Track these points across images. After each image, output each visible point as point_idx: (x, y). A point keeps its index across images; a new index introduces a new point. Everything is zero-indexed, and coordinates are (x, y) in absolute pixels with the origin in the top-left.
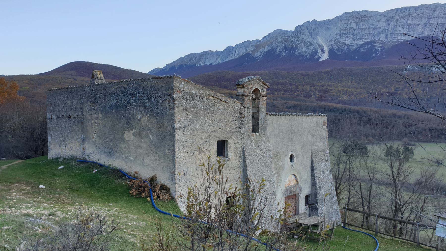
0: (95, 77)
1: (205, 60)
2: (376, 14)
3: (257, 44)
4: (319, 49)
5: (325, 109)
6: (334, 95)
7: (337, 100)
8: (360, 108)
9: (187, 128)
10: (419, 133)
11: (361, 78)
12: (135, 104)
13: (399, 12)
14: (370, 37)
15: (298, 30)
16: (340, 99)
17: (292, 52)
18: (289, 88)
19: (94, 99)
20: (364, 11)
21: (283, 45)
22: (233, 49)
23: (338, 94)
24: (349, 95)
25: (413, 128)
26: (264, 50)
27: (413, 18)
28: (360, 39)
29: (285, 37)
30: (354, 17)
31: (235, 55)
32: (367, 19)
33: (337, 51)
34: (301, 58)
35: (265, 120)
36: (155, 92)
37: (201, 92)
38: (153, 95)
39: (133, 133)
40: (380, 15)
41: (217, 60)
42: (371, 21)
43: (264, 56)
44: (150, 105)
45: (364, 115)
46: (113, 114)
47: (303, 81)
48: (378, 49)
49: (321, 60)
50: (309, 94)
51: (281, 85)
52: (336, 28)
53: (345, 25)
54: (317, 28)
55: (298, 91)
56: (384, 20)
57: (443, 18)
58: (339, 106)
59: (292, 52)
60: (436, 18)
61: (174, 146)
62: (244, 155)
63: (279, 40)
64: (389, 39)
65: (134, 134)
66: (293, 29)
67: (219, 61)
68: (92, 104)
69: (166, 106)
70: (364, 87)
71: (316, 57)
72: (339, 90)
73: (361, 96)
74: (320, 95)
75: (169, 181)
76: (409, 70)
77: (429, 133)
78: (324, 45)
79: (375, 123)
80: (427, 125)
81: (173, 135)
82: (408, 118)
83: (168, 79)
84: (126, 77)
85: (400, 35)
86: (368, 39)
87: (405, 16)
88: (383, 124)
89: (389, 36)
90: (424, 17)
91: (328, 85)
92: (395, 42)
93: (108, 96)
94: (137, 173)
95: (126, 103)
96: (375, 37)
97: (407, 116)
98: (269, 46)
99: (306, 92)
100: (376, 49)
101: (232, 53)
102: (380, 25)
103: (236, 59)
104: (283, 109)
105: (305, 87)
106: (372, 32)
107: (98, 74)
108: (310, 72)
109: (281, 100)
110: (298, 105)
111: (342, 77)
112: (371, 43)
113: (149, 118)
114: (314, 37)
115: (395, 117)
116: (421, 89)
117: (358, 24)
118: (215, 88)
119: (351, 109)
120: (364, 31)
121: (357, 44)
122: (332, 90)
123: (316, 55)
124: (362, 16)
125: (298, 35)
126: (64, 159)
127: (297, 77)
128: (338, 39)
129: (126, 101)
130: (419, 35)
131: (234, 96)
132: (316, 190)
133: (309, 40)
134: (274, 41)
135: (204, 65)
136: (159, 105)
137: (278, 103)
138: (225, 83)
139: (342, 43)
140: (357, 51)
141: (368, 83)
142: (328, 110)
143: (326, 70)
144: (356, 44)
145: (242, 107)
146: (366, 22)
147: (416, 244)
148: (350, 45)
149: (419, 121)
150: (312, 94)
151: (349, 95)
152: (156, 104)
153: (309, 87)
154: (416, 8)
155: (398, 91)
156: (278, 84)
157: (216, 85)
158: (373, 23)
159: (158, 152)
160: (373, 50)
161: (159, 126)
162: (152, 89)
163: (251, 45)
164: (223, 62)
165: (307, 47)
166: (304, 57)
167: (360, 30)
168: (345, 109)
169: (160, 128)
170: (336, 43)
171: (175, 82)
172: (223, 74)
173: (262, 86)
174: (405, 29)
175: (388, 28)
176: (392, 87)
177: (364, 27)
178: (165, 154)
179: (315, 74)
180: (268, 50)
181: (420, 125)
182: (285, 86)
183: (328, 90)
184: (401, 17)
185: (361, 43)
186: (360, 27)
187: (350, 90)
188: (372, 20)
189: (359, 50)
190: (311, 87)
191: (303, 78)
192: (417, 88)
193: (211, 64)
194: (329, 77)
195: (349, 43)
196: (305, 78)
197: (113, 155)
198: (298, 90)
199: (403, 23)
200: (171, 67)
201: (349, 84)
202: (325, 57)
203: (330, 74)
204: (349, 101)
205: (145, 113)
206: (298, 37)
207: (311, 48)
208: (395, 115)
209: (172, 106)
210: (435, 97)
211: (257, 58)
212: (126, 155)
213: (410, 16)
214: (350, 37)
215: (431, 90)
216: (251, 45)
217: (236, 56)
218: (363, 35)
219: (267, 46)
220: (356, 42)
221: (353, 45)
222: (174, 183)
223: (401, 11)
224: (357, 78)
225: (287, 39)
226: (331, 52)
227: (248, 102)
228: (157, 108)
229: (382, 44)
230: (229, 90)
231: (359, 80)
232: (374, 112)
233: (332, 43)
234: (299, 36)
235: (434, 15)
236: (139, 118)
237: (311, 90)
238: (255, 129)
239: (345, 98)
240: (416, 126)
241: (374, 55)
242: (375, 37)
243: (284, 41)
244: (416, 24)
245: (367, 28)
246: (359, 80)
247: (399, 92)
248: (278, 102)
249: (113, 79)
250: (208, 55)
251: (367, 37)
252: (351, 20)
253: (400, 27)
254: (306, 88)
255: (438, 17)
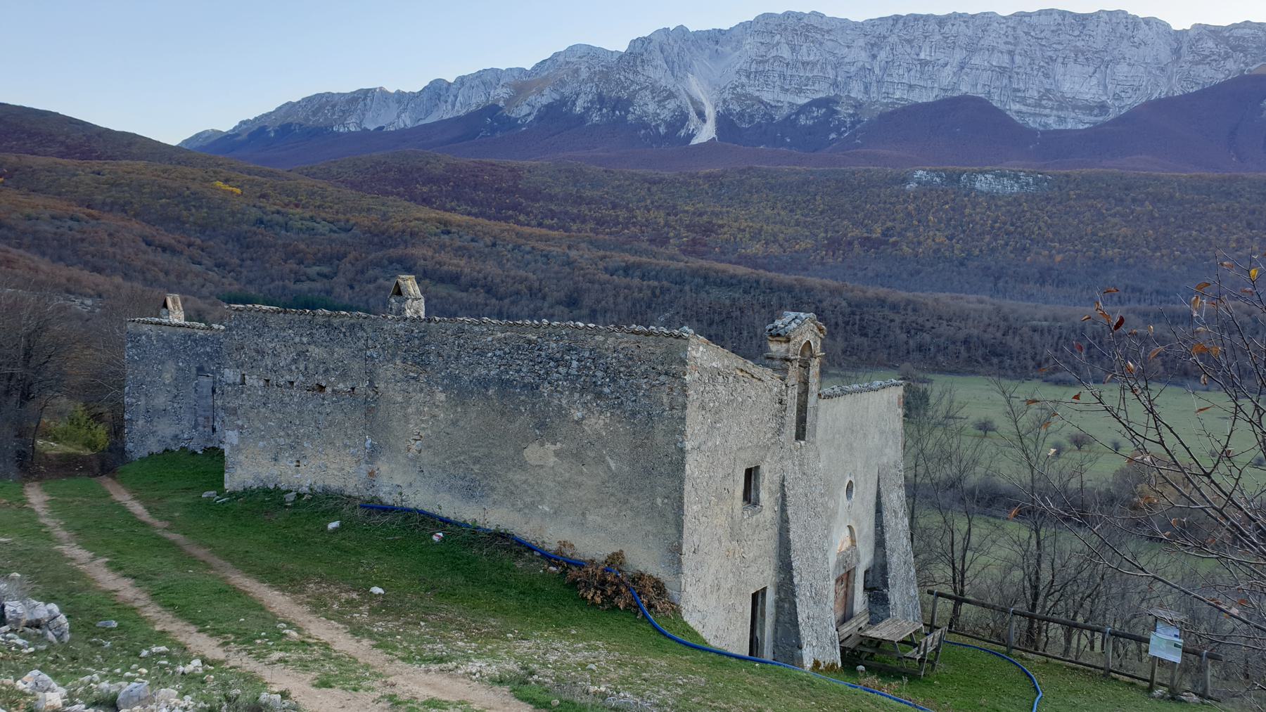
0: (405, 294)
1: (363, 114)
2: (845, 25)
3: (522, 82)
4: (691, 109)
5: (705, 278)
6: (727, 241)
7: (736, 255)
8: (796, 280)
9: (703, 447)
10: (938, 351)
11: (799, 199)
12: (565, 383)
13: (900, 25)
14: (825, 85)
15: (637, 50)
16: (743, 251)
17: (617, 112)
18: (611, 215)
19: (416, 354)
20: (814, 13)
21: (594, 90)
22: (447, 90)
23: (738, 239)
24: (766, 243)
25: (927, 337)
26: (539, 100)
27: (934, 47)
28: (799, 91)
29: (601, 68)
30: (786, 29)
31: (453, 105)
32: (819, 36)
33: (739, 119)
34: (643, 132)
35: (816, 409)
36: (630, 363)
37: (726, 362)
38: (622, 369)
39: (554, 451)
40: (853, 30)
41: (398, 117)
42: (832, 43)
43: (539, 118)
44: (612, 393)
45: (806, 298)
46: (488, 398)
47: (647, 197)
48: (845, 122)
49: (695, 142)
50: (662, 235)
51: (587, 204)
52: (737, 53)
53: (763, 49)
54: (688, 49)
55: (634, 224)
56: (861, 42)
57: (1002, 53)
58: (741, 270)
59: (617, 112)
60: (987, 52)
61: (680, 490)
62: (784, 496)
63: (584, 74)
64: (874, 95)
65: (557, 454)
66: (623, 48)
67: (406, 121)
68: (411, 365)
69: (661, 398)
70: (805, 223)
71: (683, 133)
72: (742, 227)
73: (797, 246)
74: (691, 238)
75: (662, 567)
76: (919, 183)
77: (962, 351)
78: (704, 101)
79: (833, 321)
80: (960, 329)
81: (678, 467)
82: (914, 310)
83: (671, 338)
84: (109, 154)
85: (899, 87)
86: (819, 91)
87: (914, 40)
88: (853, 325)
89: (874, 89)
90: (959, 46)
91: (713, 213)
92: (887, 104)
93: (468, 353)
94: (564, 544)
95: (534, 379)
96: (837, 87)
97: (911, 306)
98: (555, 90)
99: (654, 229)
100: (839, 120)
101: (446, 102)
102: (851, 55)
103: (458, 120)
104: (594, 275)
105: (652, 214)
106: (831, 74)
107: (409, 287)
108: (667, 174)
109: (589, 250)
110: (639, 266)
111: (749, 192)
112: (827, 103)
113: (608, 421)
114: (679, 74)
115: (883, 307)
116: (946, 234)
117: (797, 48)
118: (395, 201)
119: (772, 280)
120: (812, 70)
121: (791, 104)
122: (722, 226)
123: (682, 126)
124: (808, 27)
125: (635, 64)
126: (299, 496)
127: (632, 184)
128: (743, 86)
129: (534, 372)
130: (946, 90)
131: (453, 230)
132: (885, 555)
133: (666, 81)
134: (569, 78)
135: (359, 129)
136: (641, 394)
137: (582, 257)
138: (425, 189)
139: (753, 98)
140: (790, 121)
141: (817, 213)
142: (715, 283)
143: (708, 171)
144: (789, 103)
145: (784, 387)
146: (818, 46)
147: (1102, 672)
148: (773, 104)
149: (940, 318)
150: (672, 234)
151: (765, 243)
152: (632, 391)
153: (663, 215)
154: (941, 21)
155: (891, 236)
156: (579, 200)
157: (398, 194)
158: (835, 49)
159: (632, 500)
160: (831, 122)
161: (639, 442)
162: (621, 356)
163: (501, 83)
164: (416, 125)
165: (659, 102)
166: (652, 130)
167: (800, 65)
168: (758, 282)
169: (641, 446)
170: (738, 98)
171: (689, 349)
172: (420, 161)
173: (816, 334)
174: (912, 73)
175: (872, 65)
176: (875, 226)
177: (812, 58)
178: (653, 506)
179: (681, 179)
180: (551, 101)
181: (943, 328)
182: (600, 208)
183: (714, 225)
184: (906, 40)
185: (802, 100)
186: (802, 56)
187: (769, 228)
188: (832, 40)
189: (795, 119)
190: (668, 214)
191: (649, 189)
192: (937, 230)
193: (381, 128)
194: (715, 190)
195: (772, 98)
196: (654, 189)
197: (482, 496)
198: (634, 223)
199: (907, 57)
200: (254, 129)
201: (768, 212)
202: (706, 133)
203: (718, 183)
204: (765, 258)
205: (599, 408)
206: (636, 73)
207: (669, 106)
208: (882, 302)
209: (680, 400)
210: (978, 256)
211: (519, 122)
212: (528, 500)
213: (927, 40)
214: (774, 82)
215: (969, 239)
216: (501, 83)
217: (458, 111)
218: (808, 79)
219: (548, 89)
220: (789, 98)
221: (782, 107)
222: (678, 574)
223: (904, 24)
224: (789, 197)
225: (605, 75)
226: (724, 122)
227: (794, 372)
228: (633, 401)
229: (856, 107)
230: (436, 209)
231: (794, 202)
232: (830, 292)
233: (727, 96)
234: (639, 69)
235: (982, 42)
236: (576, 418)
237: (667, 224)
238: (800, 435)
239: (756, 248)
240: (933, 330)
241: (833, 136)
242: (837, 87)
243: (596, 80)
244: (939, 62)
245: (818, 61)
246: (794, 202)
247: (892, 240)
248: (581, 253)
249: (62, 157)
250: (372, 100)
251: (817, 85)
252: (779, 36)
253: (900, 65)
254: (655, 218)
255: (992, 50)
